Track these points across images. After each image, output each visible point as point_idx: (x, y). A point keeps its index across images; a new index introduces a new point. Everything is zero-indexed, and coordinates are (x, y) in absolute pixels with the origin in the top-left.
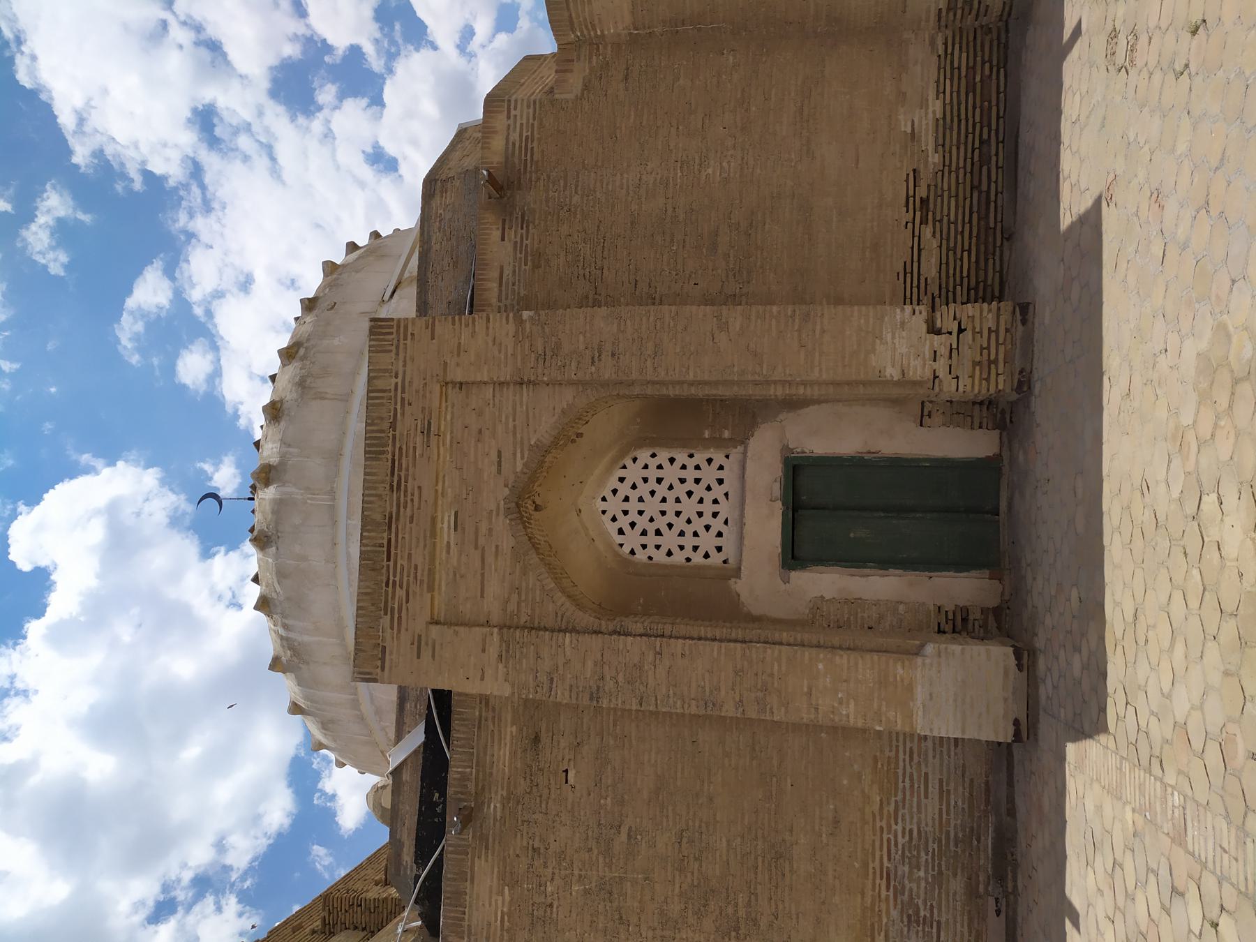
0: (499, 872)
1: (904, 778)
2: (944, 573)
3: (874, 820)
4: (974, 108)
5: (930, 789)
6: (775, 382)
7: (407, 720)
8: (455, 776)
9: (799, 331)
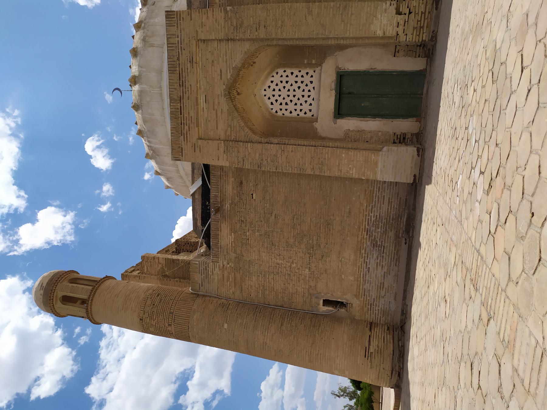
2: (398, 120)
6: (331, 38)
7: (195, 176)
8: (213, 196)
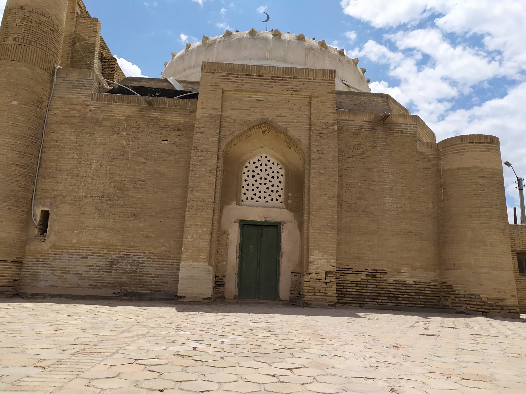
0: (131, 115)
1: (163, 262)
2: (237, 279)
3: (148, 250)
4: (410, 295)
5: (159, 271)
6: (309, 217)
7: (185, 84)
8: (166, 100)
9: (328, 225)
